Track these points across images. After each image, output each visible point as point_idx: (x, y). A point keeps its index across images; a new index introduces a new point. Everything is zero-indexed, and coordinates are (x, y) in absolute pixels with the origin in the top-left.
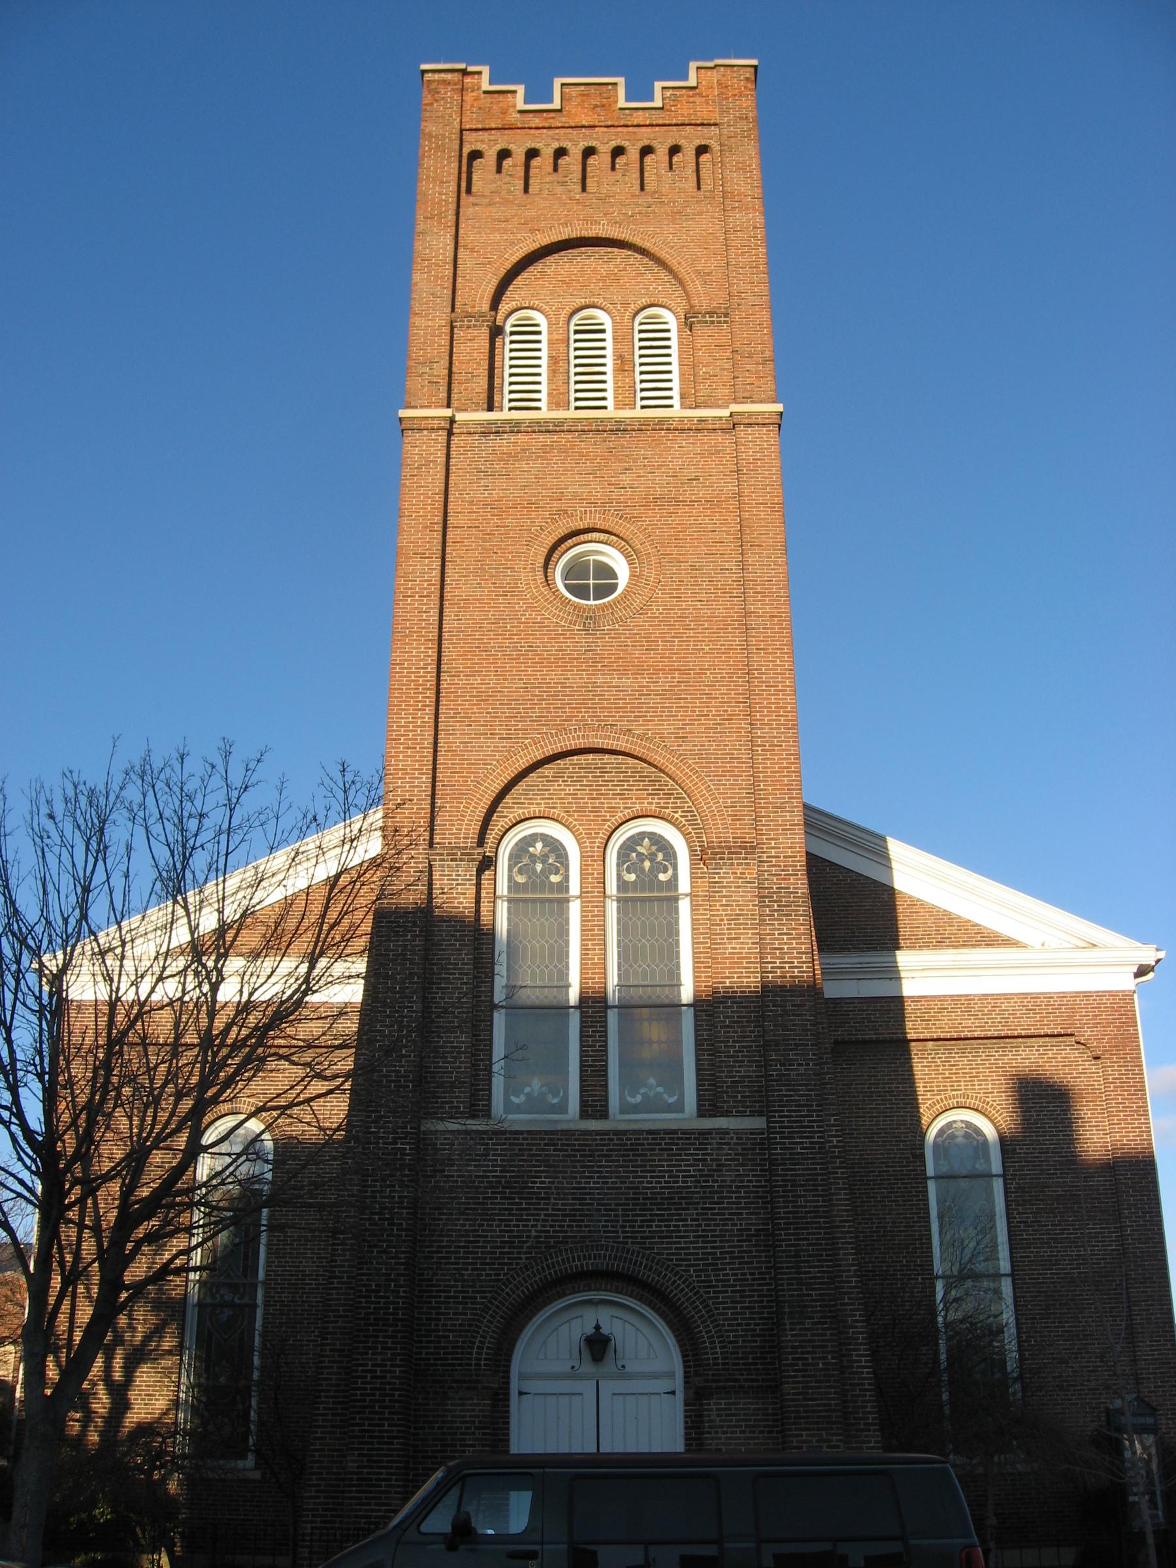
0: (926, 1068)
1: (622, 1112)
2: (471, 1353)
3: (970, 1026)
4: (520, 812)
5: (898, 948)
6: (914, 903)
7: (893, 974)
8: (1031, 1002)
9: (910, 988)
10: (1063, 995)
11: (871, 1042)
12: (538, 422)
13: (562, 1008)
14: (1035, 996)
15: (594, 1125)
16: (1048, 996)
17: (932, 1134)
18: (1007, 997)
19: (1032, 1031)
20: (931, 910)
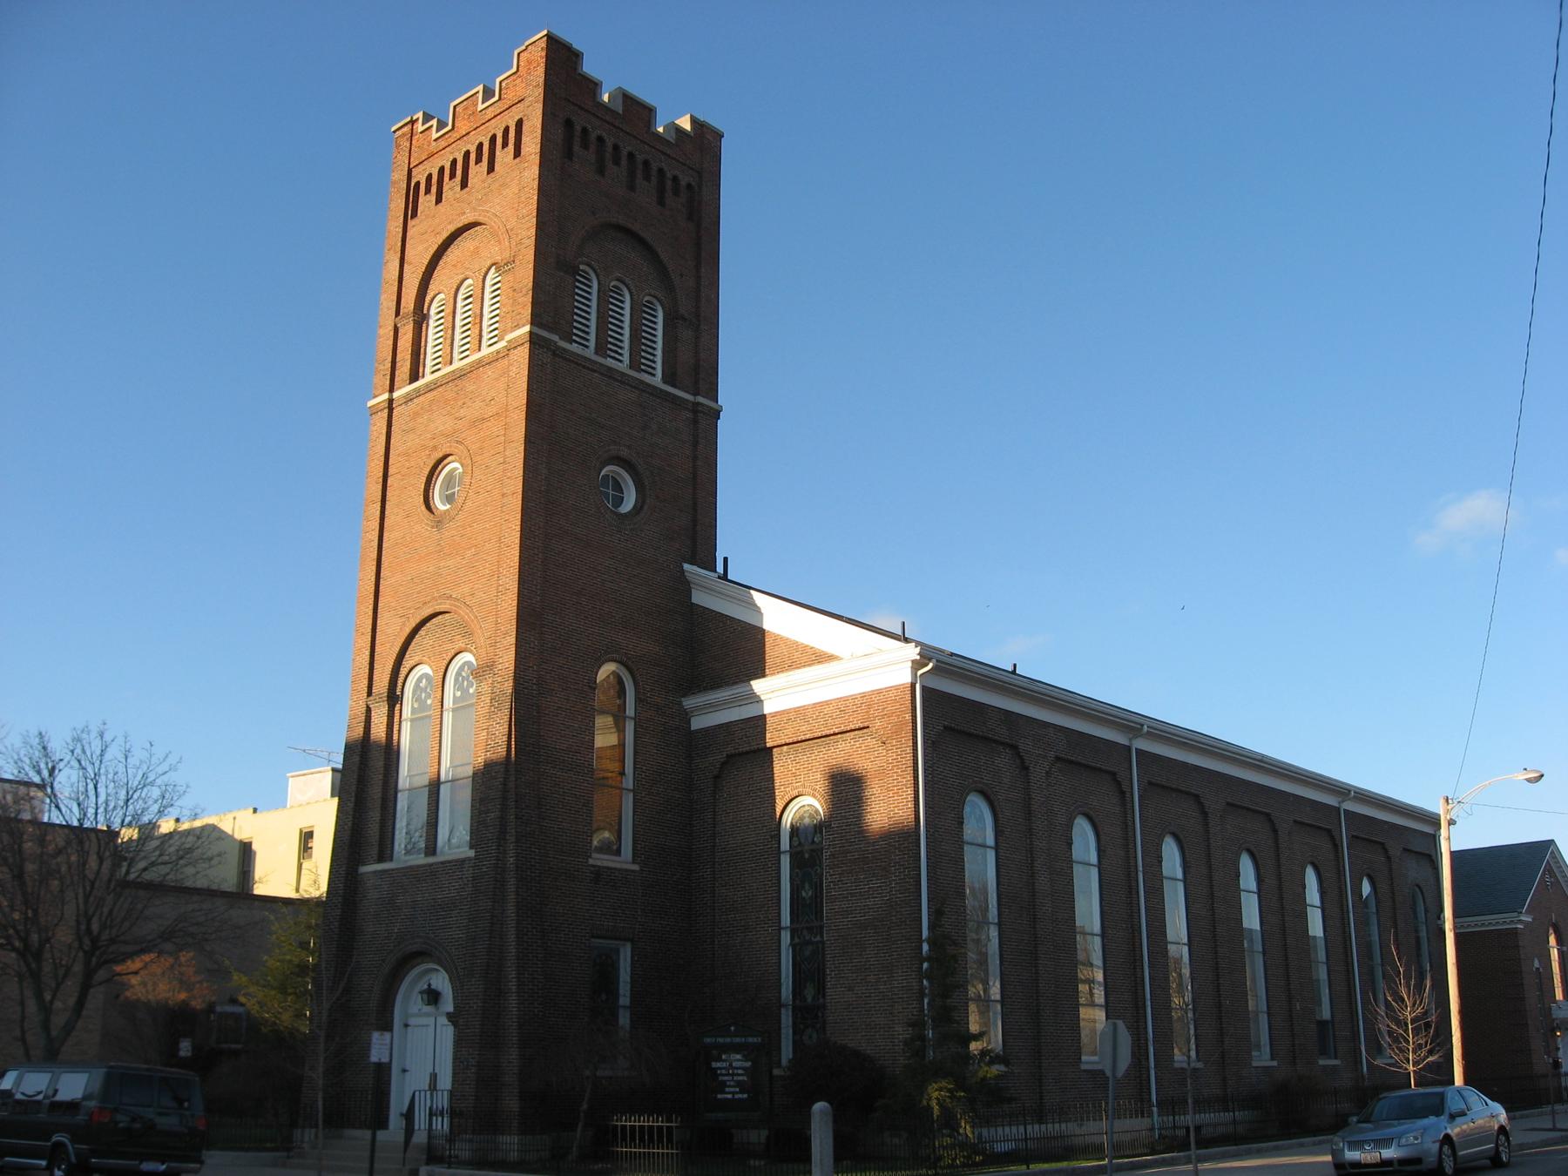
0: (782, 767)
1: (408, 852)
2: (633, 1127)
3: (805, 731)
4: (412, 663)
5: (760, 673)
6: (777, 637)
7: (758, 701)
8: (843, 704)
9: (768, 708)
10: (863, 695)
11: (747, 753)
12: (427, 385)
13: (507, 771)
14: (845, 699)
15: (431, 860)
16: (854, 697)
17: (788, 819)
18: (827, 703)
19: (843, 728)
20: (785, 640)
